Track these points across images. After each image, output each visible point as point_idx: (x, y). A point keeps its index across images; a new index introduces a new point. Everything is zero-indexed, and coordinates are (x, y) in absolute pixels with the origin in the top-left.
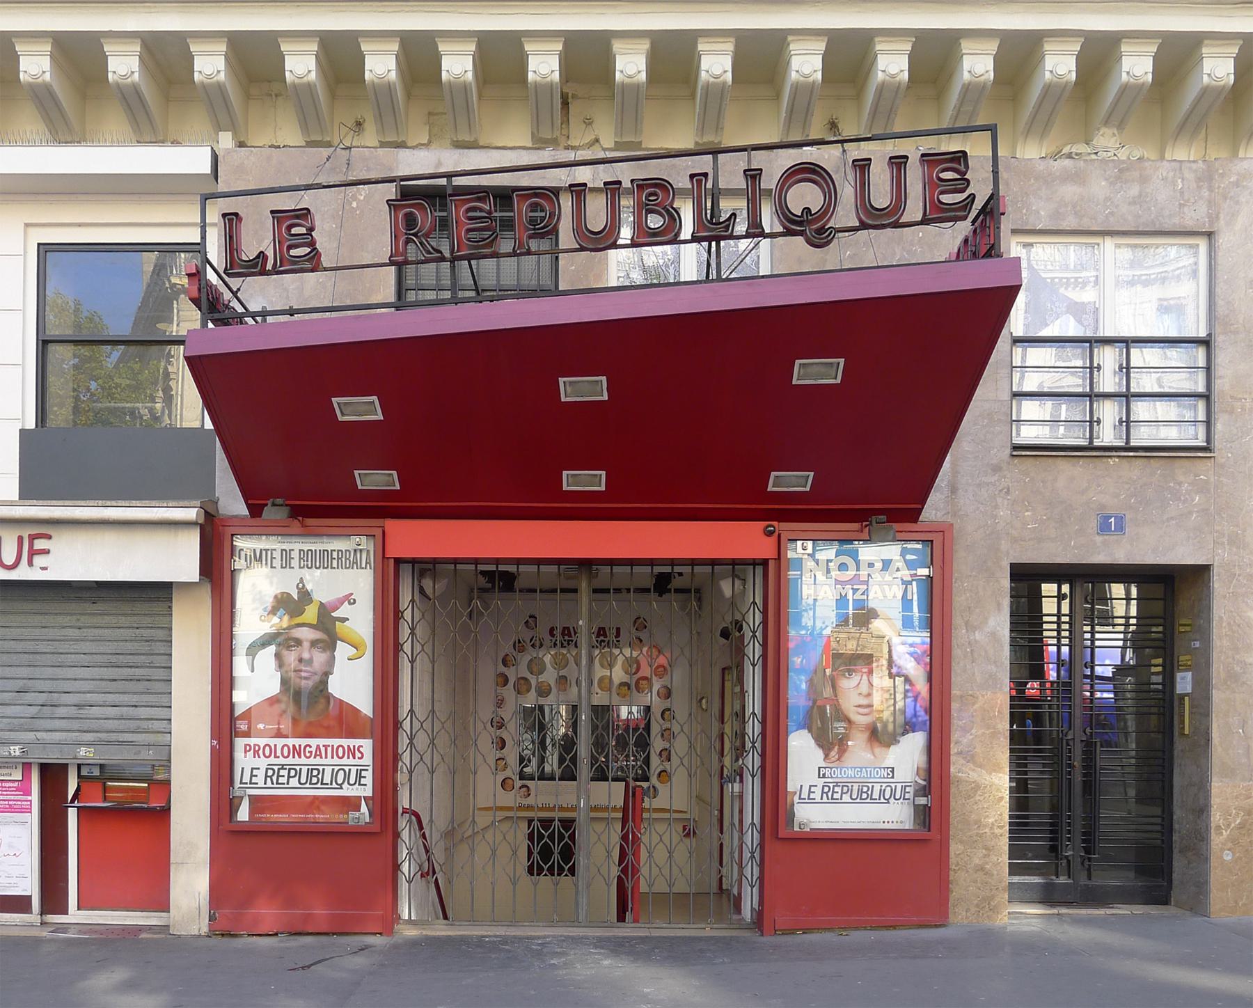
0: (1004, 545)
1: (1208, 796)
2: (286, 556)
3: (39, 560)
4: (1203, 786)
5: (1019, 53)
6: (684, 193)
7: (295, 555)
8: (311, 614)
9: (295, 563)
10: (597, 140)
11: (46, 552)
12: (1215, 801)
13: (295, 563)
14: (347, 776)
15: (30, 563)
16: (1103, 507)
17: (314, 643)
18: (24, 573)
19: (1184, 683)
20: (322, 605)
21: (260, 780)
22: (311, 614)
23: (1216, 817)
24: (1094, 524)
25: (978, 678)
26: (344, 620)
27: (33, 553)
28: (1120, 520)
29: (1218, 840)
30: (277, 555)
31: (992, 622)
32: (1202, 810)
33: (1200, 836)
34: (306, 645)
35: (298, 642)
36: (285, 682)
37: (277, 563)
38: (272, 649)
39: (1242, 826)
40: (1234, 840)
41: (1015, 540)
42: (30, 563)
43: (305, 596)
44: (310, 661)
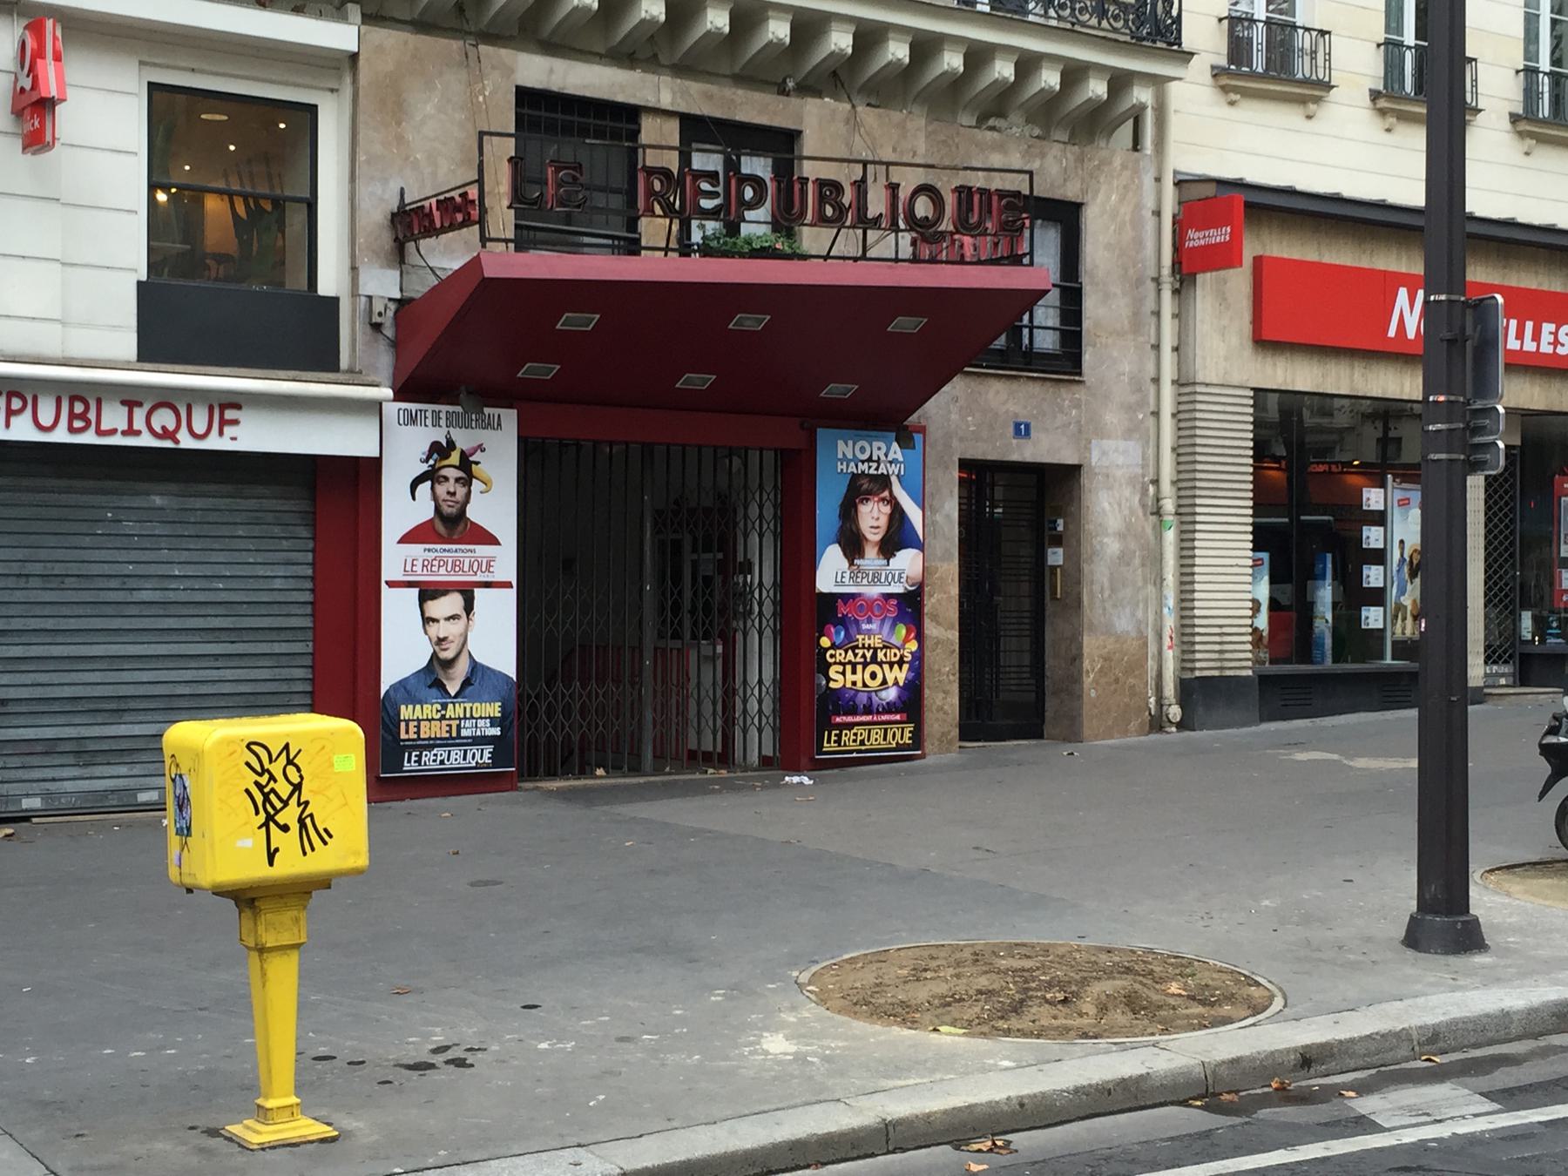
0: (955, 443)
1: (1080, 647)
2: (436, 415)
3: (229, 431)
4: (1075, 640)
5: (869, 37)
6: (1409, 48)
7: (443, 415)
8: (455, 458)
9: (443, 422)
10: (655, 56)
11: (235, 422)
12: (1086, 650)
13: (443, 422)
14: (480, 565)
15: (221, 433)
16: (1016, 415)
17: (457, 480)
18: (214, 443)
19: (1055, 556)
20: (462, 452)
21: (418, 568)
22: (455, 458)
23: (1086, 664)
24: (1011, 429)
25: (939, 553)
26: (477, 463)
27: (224, 423)
28: (1027, 426)
29: (1088, 680)
30: (429, 414)
31: (947, 506)
32: (1076, 658)
33: (1074, 678)
34: (452, 481)
35: (446, 479)
36: (437, 509)
37: (429, 422)
38: (429, 483)
39: (1101, 670)
40: (1096, 681)
41: (961, 440)
42: (221, 433)
43: (451, 445)
44: (454, 494)
